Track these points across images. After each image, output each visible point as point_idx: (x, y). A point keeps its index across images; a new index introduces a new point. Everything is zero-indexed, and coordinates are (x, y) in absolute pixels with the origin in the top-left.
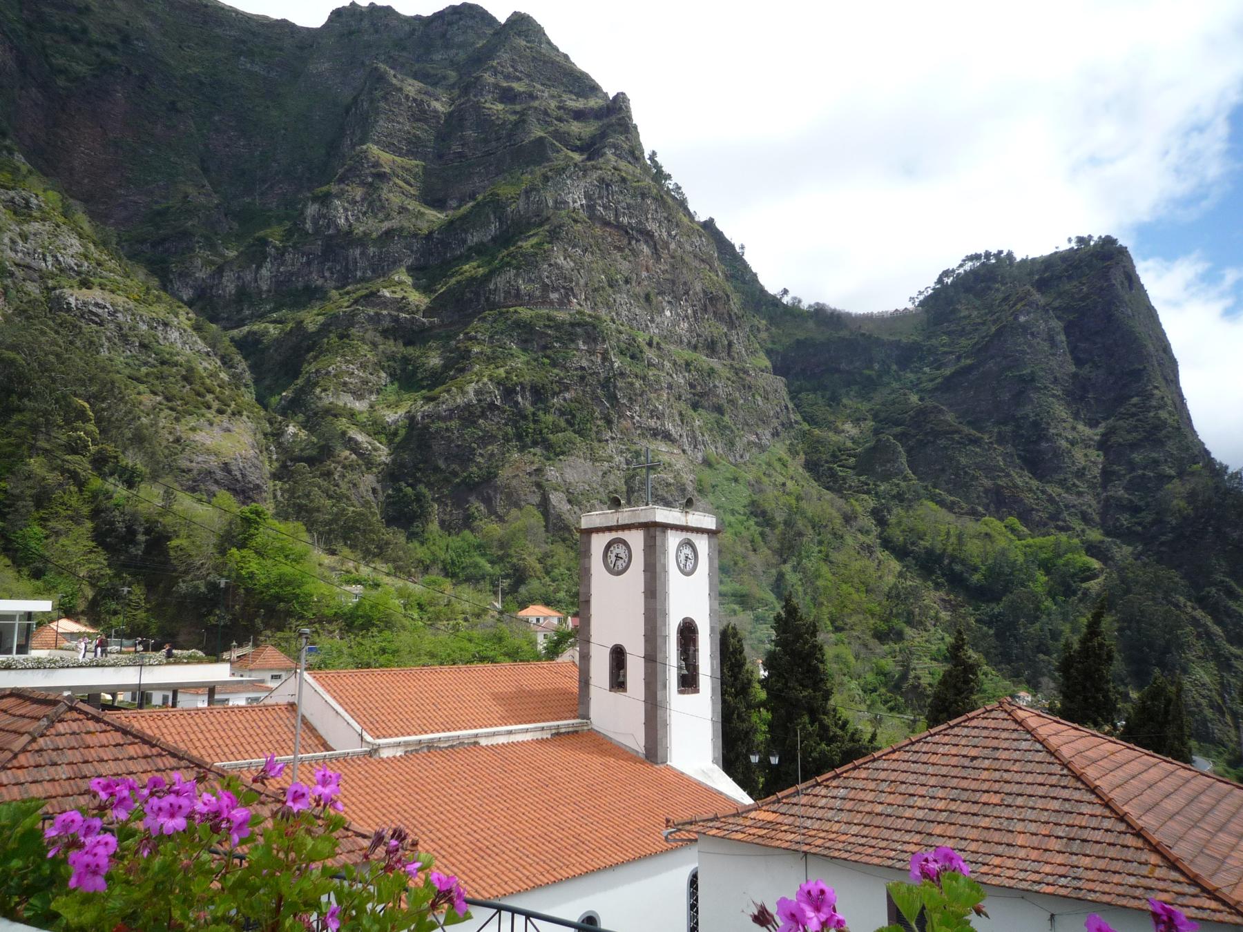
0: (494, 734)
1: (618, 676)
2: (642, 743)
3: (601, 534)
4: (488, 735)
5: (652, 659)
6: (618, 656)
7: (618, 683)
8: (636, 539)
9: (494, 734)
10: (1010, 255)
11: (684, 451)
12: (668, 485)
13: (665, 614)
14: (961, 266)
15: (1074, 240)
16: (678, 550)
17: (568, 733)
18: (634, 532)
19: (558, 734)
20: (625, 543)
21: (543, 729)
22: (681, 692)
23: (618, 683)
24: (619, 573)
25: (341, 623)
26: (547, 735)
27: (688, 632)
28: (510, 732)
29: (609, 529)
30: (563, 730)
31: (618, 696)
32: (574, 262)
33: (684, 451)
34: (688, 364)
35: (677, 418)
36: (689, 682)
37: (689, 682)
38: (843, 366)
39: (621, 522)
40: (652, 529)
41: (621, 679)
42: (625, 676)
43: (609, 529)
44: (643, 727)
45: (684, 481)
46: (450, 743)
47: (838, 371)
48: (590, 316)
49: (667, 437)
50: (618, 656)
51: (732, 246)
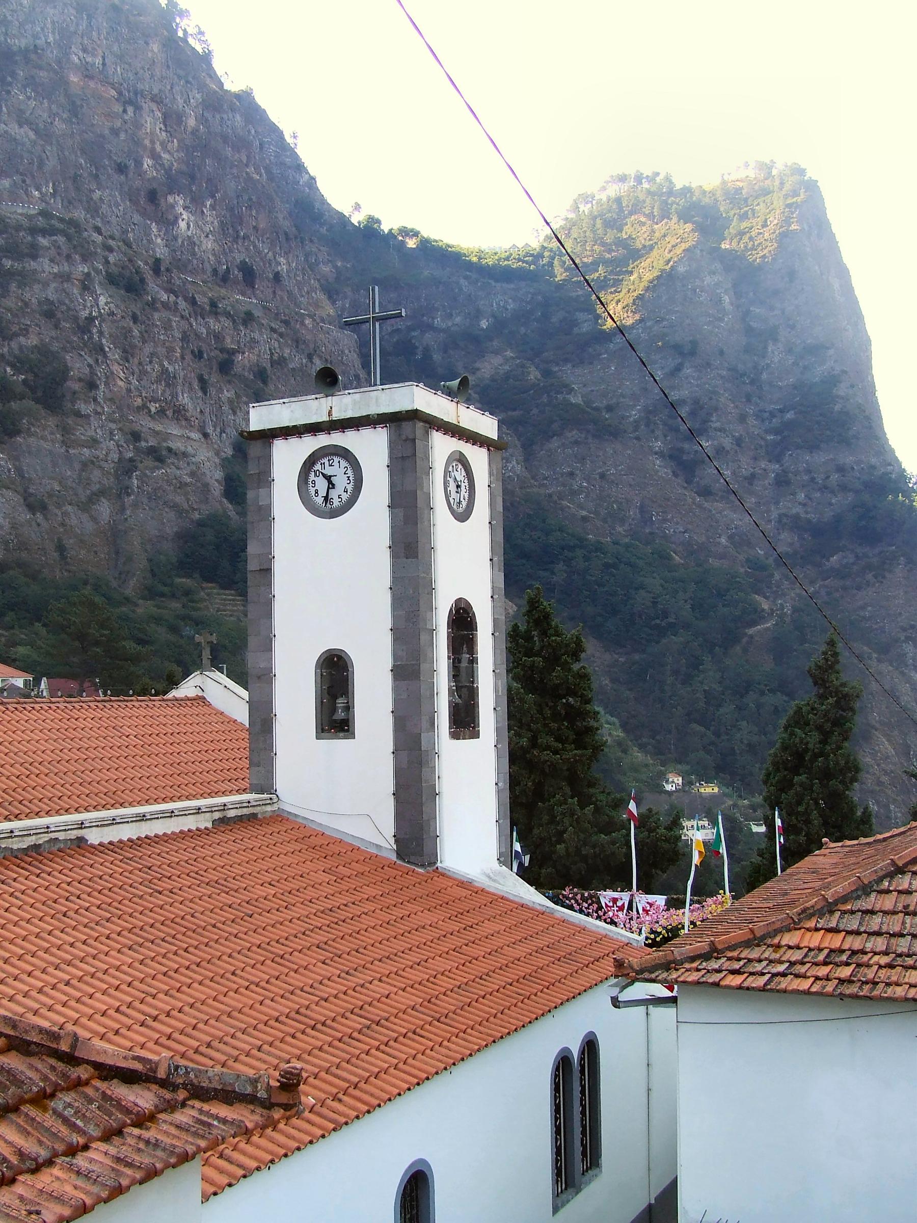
0: (113, 822)
1: (334, 710)
2: (389, 828)
3: (293, 441)
4: (102, 824)
5: (408, 671)
6: (335, 673)
7: (335, 720)
8: (372, 449)
9: (113, 822)
10: (668, 179)
11: (206, 435)
12: (183, 485)
13: (430, 589)
14: (604, 189)
15: (752, 165)
16: (447, 473)
17: (240, 819)
18: (367, 433)
19: (223, 821)
20: (345, 454)
21: (199, 811)
22: (455, 736)
23: (335, 720)
24: (334, 514)
25: (190, 267)
26: (205, 822)
27: (462, 620)
28: (142, 818)
29: (314, 429)
30: (232, 814)
31: (339, 745)
32: (37, 132)
33: (206, 435)
34: (213, 304)
35: (196, 385)
36: (464, 721)
37: (464, 721)
38: (438, 322)
39: (336, 416)
40: (407, 426)
41: (340, 715)
42: (349, 708)
43: (314, 429)
44: (390, 803)
45: (208, 479)
46: (31, 841)
47: (431, 327)
48: (61, 220)
49: (179, 414)
50: (335, 673)
51: (280, 134)
